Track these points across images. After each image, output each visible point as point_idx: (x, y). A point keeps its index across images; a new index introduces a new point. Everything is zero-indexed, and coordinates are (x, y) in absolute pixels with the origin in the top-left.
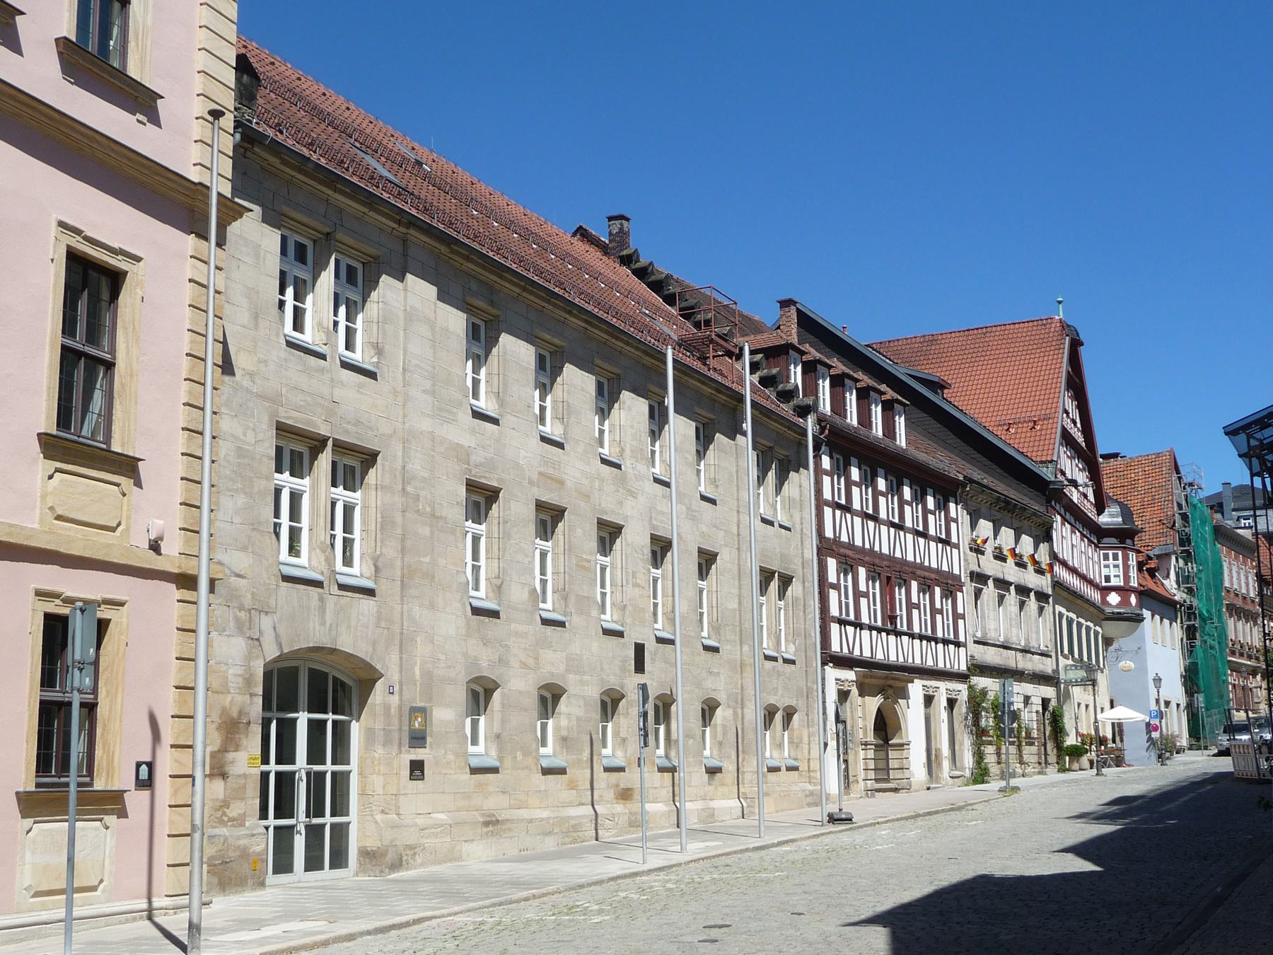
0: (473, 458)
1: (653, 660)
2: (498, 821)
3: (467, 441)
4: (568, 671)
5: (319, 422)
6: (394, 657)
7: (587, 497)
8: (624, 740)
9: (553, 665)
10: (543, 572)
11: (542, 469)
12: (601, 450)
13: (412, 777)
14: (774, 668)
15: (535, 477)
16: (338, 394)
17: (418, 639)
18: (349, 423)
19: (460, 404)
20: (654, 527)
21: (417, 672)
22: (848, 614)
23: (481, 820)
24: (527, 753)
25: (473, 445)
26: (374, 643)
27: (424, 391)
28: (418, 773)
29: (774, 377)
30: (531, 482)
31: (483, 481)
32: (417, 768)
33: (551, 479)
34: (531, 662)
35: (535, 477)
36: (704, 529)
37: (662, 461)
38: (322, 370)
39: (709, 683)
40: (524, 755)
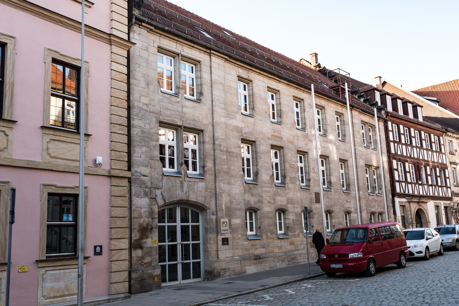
0: (244, 131)
3: (240, 125)
4: (288, 203)
6: (213, 202)
7: (292, 143)
8: (334, 226)
9: (281, 201)
10: (343, 179)
11: (273, 134)
13: (228, 244)
15: (270, 136)
16: (185, 110)
17: (223, 195)
18: (190, 120)
19: (237, 112)
22: (414, 181)
24: (272, 233)
25: (243, 126)
27: (221, 108)
28: (226, 242)
30: (268, 138)
32: (225, 241)
34: (272, 201)
35: (270, 136)
36: (341, 152)
37: (323, 129)
38: (178, 102)
39: (347, 205)
40: (271, 234)
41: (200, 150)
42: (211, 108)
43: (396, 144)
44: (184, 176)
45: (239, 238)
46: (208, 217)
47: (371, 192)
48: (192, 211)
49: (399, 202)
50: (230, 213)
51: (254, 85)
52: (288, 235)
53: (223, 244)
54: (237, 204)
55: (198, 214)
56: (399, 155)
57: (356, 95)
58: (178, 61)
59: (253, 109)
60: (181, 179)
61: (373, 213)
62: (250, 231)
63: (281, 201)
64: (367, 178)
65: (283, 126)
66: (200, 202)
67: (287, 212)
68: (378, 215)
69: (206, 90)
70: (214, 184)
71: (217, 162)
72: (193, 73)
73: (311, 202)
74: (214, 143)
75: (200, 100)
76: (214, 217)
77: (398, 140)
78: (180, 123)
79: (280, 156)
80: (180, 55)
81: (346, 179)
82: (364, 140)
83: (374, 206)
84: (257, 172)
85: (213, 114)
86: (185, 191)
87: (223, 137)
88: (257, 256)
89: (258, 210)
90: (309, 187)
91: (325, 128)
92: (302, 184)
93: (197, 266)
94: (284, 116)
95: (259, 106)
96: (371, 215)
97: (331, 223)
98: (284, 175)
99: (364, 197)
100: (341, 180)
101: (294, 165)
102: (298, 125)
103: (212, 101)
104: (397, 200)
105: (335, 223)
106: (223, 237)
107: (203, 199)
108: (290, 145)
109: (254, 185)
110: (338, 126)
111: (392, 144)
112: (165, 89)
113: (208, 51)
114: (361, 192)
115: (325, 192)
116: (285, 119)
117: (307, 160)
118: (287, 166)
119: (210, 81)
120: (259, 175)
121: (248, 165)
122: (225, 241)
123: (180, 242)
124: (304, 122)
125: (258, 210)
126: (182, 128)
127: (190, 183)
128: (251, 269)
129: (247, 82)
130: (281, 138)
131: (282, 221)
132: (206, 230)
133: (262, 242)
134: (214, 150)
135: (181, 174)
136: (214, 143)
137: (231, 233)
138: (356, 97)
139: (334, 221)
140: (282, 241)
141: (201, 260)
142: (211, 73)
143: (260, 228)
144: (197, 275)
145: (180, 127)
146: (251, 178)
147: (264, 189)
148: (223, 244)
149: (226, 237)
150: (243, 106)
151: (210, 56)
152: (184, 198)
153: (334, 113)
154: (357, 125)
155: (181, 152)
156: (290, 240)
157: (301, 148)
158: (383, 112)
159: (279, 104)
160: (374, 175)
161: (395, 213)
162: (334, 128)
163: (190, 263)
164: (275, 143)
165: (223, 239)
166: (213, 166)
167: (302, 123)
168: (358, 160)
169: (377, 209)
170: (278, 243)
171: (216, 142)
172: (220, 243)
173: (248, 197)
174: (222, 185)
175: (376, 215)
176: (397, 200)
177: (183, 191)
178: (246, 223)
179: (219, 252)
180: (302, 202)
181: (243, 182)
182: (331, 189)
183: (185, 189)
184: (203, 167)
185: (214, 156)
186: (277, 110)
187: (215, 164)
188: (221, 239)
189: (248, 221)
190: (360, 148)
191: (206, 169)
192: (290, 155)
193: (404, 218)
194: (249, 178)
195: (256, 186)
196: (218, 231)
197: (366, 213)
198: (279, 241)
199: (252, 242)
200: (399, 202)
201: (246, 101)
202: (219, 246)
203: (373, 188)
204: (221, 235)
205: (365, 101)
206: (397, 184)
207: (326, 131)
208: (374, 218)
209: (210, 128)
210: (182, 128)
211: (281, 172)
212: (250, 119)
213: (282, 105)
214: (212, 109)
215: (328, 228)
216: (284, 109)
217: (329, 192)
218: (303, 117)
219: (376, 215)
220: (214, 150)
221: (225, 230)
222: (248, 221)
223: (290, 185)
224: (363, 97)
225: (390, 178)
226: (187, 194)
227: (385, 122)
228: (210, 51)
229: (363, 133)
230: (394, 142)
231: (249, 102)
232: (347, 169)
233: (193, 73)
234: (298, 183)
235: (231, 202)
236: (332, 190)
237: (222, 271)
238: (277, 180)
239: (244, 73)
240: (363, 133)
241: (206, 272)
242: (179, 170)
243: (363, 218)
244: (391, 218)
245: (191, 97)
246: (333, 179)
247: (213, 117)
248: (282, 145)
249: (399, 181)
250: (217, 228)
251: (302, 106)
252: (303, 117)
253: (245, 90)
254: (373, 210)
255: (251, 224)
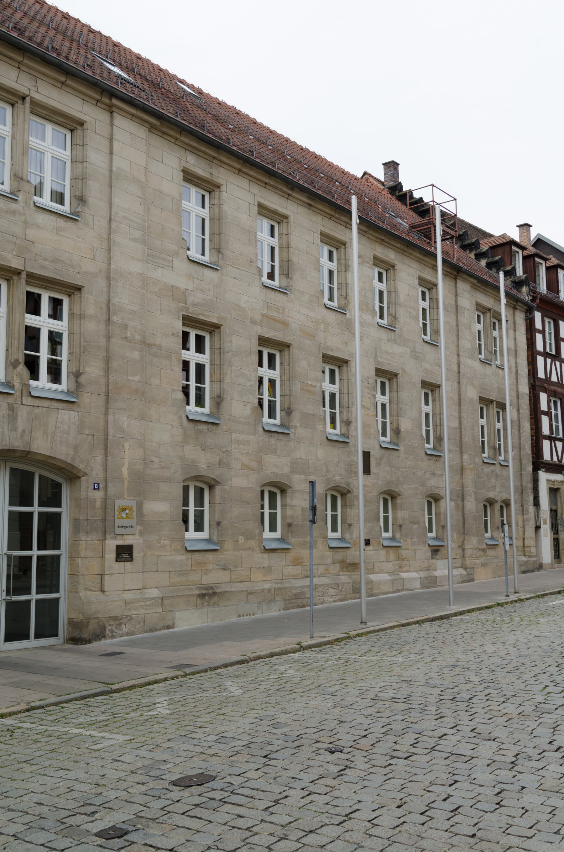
0: (190, 299)
1: (378, 465)
2: (214, 594)
3: (182, 283)
4: (293, 471)
5: (10, 256)
6: (99, 459)
7: (312, 336)
8: (400, 526)
9: (276, 465)
10: (427, 425)
11: (265, 312)
12: (480, 356)
13: (130, 558)
14: (493, 471)
15: (258, 317)
16: (32, 233)
17: (127, 445)
18: (46, 259)
19: (175, 254)
20: (379, 363)
21: (125, 472)
22: (558, 433)
23: (197, 592)
24: (249, 536)
25: (190, 287)
26: (76, 448)
27: (134, 240)
28: (125, 556)
29: (496, 262)
30: (254, 322)
31: (201, 317)
32: (124, 553)
33: (275, 320)
34: (254, 464)
35: (258, 317)
36: (427, 366)
37: (389, 314)
38: (14, 212)
39: (432, 482)
40: (247, 538)
41: (70, 334)
42: (106, 236)
43: (549, 361)
44: (19, 393)
45: (163, 547)
46: (83, 494)
47: (489, 458)
48: (40, 476)
49: (548, 480)
50: (141, 485)
51: (224, 195)
52: (288, 543)
53: (118, 559)
54: (163, 468)
55: (57, 487)
56: (553, 383)
57: (471, 251)
58: (22, 114)
59: (219, 251)
60: (10, 400)
61: (491, 502)
62: (270, 531)
63: (277, 466)
64: (482, 427)
65: (293, 296)
66: (63, 457)
67: (289, 491)
68: (502, 507)
69: (95, 192)
70: (102, 416)
71: (114, 364)
72: (203, 207)
73: (351, 470)
74: (109, 321)
75: (288, 288)
76: (99, 495)
77: (554, 352)
78: (16, 264)
79: (281, 363)
80: (28, 99)
81: (435, 426)
82: (480, 345)
83: (494, 488)
84: (219, 396)
85: (109, 250)
86: (20, 429)
87: (135, 309)
88: (206, 589)
89: (218, 483)
90: (348, 438)
91: (393, 312)
92: (382, 439)
93: (48, 611)
94: (296, 276)
95: (234, 245)
96: (485, 506)
97: (394, 519)
98: (289, 408)
99: (472, 466)
100: (424, 428)
101: (315, 387)
102: (381, 317)
103: (110, 220)
104: (543, 476)
105: (404, 519)
106: (121, 542)
107: (71, 452)
108: (307, 342)
109: (210, 426)
110: (424, 310)
111: (540, 360)
112: (194, 254)
113: (106, 100)
114: (466, 457)
115: (383, 451)
116: (298, 282)
117: (345, 378)
118: (297, 387)
119: (107, 173)
120: (224, 404)
121: (200, 378)
122: (124, 553)
123: (5, 550)
124: (344, 294)
125: (218, 483)
126: (23, 275)
127: (37, 411)
128: (188, 620)
129: (278, 219)
130: (286, 324)
131: (279, 511)
132: (76, 525)
133: (221, 556)
134: (108, 337)
135: (13, 387)
136: (109, 321)
137: (141, 533)
138: (472, 255)
139: (400, 514)
140: (274, 556)
141: (63, 594)
142: (111, 153)
143: (219, 524)
144: (47, 628)
145: (18, 273)
146: (278, 421)
147: (234, 435)
148: (118, 559)
149: (127, 543)
150: (266, 270)
151: (112, 113)
152: (18, 444)
153: (417, 282)
154: (466, 312)
155: (16, 335)
156: (292, 554)
157: (332, 350)
158: (525, 289)
159: (286, 247)
160: (498, 421)
161: (537, 503)
162: (414, 313)
163: (29, 602)
164: (269, 334)
165: (118, 547)
166: (102, 373)
167: (340, 295)
168: (463, 388)
169: (497, 494)
170: (265, 559)
171: (115, 318)
172: (111, 555)
173: (192, 452)
174: (124, 421)
175: (497, 507)
176: (543, 476)
177: (16, 429)
178: (262, 514)
179: (106, 578)
180: (328, 471)
181: (180, 417)
182: (397, 445)
183: (21, 423)
184: (77, 375)
185: (108, 350)
186: (281, 261)
187: (107, 371)
188: (114, 548)
189: (267, 511)
190: (469, 361)
191: (82, 379)
192: (304, 363)
193: (556, 515)
194: (272, 421)
195: (214, 427)
196: (105, 528)
197: (473, 501)
198: (266, 555)
199: (196, 556)
200: (548, 480)
201: (273, 260)
202: (107, 564)
203: (494, 448)
204: (114, 538)
205: (489, 265)
206: (546, 444)
207: (395, 318)
208: (492, 511)
209: (101, 283)
210: (23, 275)
211: (281, 401)
212: (208, 273)
213: (292, 250)
214: (109, 240)
215: (431, 531)
216: (297, 259)
217: (394, 452)
218: (343, 282)
219: (497, 507)
220: (108, 337)
221: (125, 527)
222: (267, 511)
223: (301, 432)
224: (485, 257)
225: (532, 429)
226: (27, 438)
227: (529, 311)
228: (111, 100)
229: (479, 332)
230: (546, 355)
231: (212, 234)
232: (438, 404)
233: (203, 207)
234: (320, 427)
235: (146, 462)
236: (401, 448)
237: (111, 622)
238: (270, 417)
239: (200, 168)
240: (479, 332)
241: (72, 623)
242: (9, 379)
243: (466, 510)
244: (527, 514)
245: (269, 282)
246: (405, 425)
247: (109, 259)
248: (287, 340)
249: (550, 438)
250: (104, 520)
251: (343, 257)
252: (343, 282)
253: (272, 235)
254: (491, 495)
255: (273, 518)
